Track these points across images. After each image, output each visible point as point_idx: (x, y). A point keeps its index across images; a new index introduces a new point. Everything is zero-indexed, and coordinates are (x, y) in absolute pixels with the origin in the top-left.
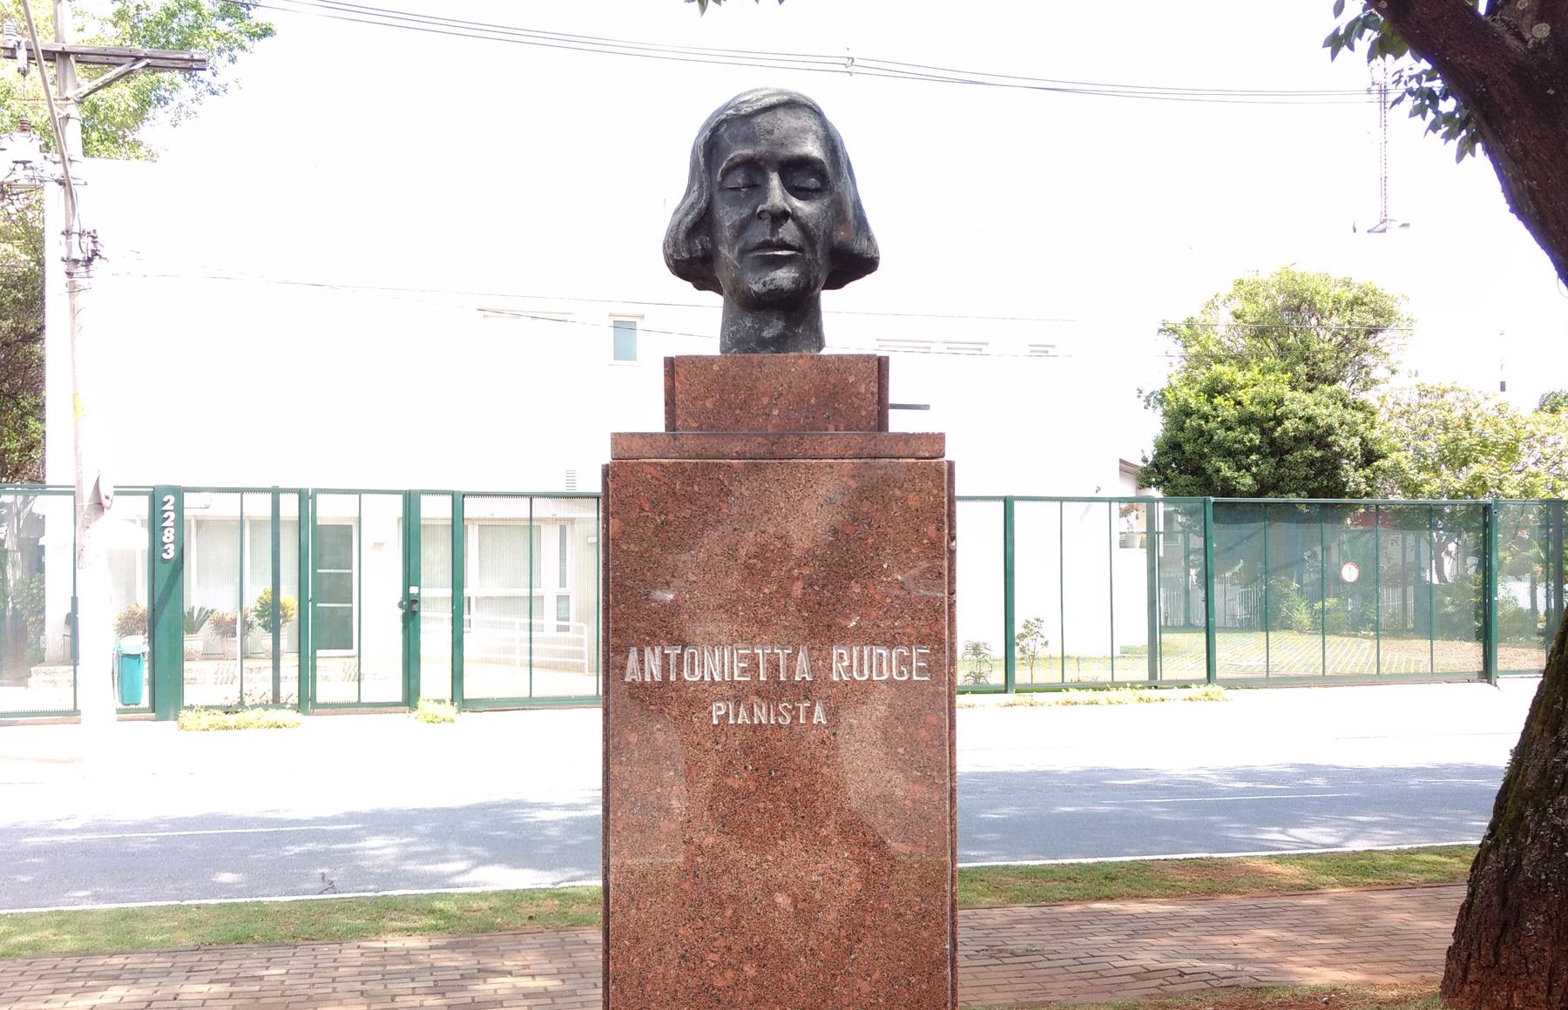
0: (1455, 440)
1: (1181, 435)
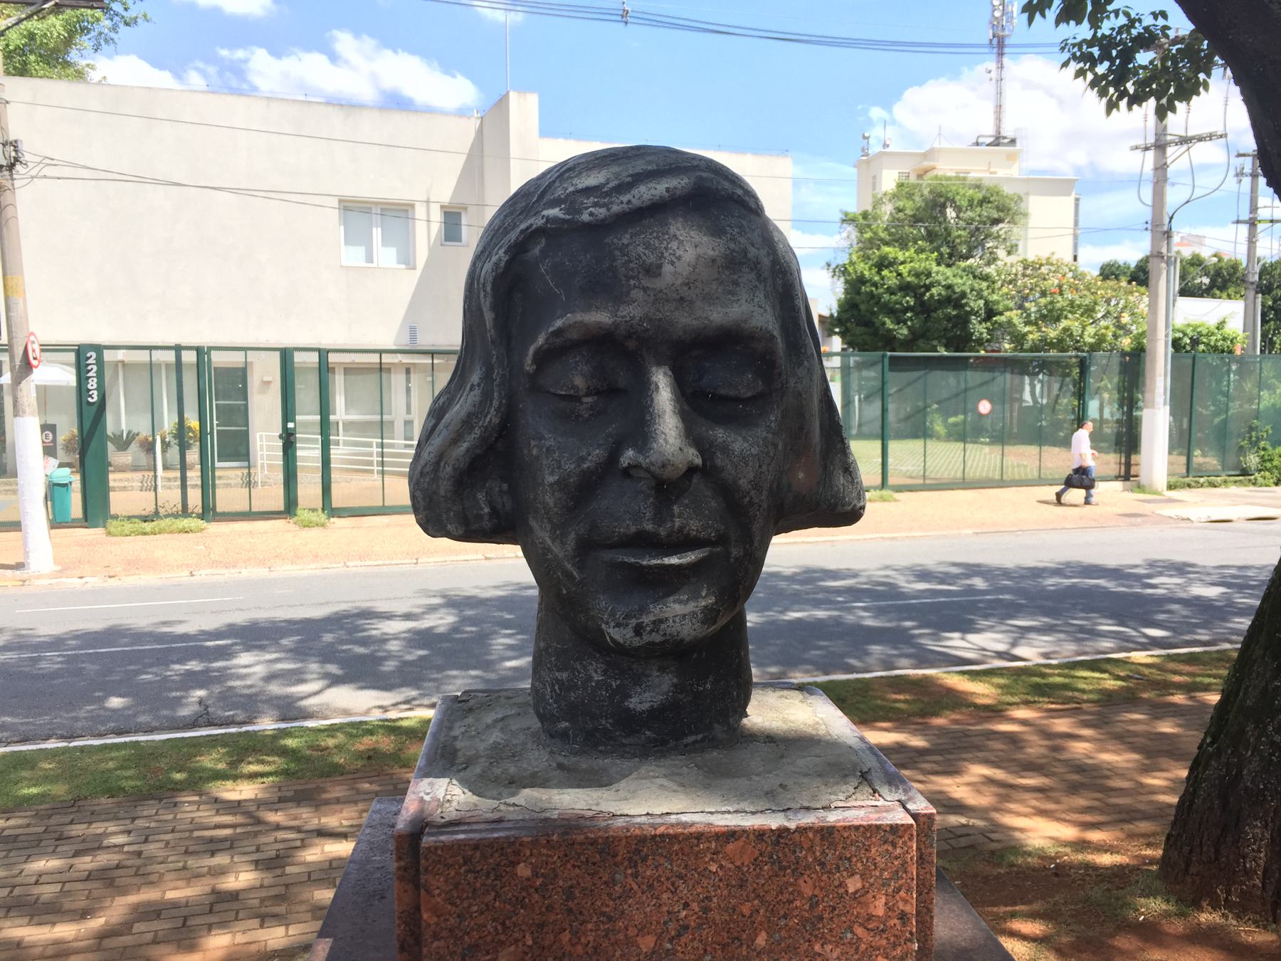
0: (1051, 303)
1: (857, 297)
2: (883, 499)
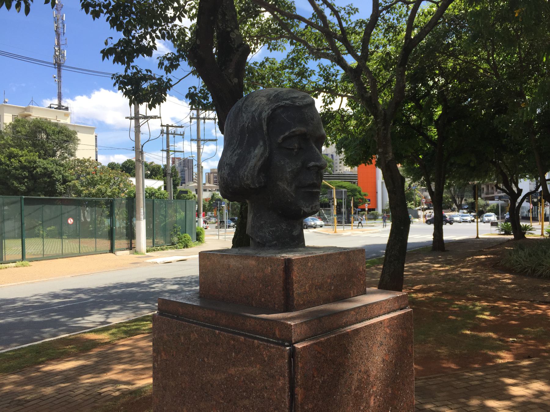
0: (92, 178)
2: (23, 266)
